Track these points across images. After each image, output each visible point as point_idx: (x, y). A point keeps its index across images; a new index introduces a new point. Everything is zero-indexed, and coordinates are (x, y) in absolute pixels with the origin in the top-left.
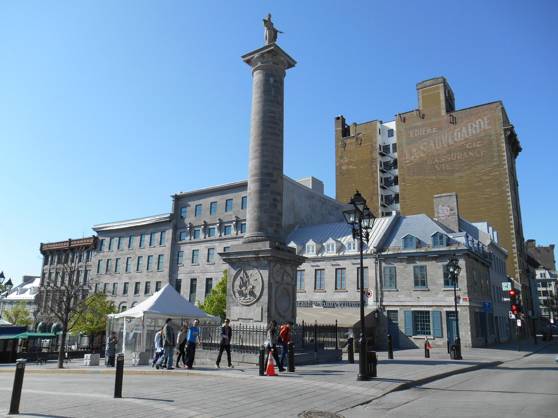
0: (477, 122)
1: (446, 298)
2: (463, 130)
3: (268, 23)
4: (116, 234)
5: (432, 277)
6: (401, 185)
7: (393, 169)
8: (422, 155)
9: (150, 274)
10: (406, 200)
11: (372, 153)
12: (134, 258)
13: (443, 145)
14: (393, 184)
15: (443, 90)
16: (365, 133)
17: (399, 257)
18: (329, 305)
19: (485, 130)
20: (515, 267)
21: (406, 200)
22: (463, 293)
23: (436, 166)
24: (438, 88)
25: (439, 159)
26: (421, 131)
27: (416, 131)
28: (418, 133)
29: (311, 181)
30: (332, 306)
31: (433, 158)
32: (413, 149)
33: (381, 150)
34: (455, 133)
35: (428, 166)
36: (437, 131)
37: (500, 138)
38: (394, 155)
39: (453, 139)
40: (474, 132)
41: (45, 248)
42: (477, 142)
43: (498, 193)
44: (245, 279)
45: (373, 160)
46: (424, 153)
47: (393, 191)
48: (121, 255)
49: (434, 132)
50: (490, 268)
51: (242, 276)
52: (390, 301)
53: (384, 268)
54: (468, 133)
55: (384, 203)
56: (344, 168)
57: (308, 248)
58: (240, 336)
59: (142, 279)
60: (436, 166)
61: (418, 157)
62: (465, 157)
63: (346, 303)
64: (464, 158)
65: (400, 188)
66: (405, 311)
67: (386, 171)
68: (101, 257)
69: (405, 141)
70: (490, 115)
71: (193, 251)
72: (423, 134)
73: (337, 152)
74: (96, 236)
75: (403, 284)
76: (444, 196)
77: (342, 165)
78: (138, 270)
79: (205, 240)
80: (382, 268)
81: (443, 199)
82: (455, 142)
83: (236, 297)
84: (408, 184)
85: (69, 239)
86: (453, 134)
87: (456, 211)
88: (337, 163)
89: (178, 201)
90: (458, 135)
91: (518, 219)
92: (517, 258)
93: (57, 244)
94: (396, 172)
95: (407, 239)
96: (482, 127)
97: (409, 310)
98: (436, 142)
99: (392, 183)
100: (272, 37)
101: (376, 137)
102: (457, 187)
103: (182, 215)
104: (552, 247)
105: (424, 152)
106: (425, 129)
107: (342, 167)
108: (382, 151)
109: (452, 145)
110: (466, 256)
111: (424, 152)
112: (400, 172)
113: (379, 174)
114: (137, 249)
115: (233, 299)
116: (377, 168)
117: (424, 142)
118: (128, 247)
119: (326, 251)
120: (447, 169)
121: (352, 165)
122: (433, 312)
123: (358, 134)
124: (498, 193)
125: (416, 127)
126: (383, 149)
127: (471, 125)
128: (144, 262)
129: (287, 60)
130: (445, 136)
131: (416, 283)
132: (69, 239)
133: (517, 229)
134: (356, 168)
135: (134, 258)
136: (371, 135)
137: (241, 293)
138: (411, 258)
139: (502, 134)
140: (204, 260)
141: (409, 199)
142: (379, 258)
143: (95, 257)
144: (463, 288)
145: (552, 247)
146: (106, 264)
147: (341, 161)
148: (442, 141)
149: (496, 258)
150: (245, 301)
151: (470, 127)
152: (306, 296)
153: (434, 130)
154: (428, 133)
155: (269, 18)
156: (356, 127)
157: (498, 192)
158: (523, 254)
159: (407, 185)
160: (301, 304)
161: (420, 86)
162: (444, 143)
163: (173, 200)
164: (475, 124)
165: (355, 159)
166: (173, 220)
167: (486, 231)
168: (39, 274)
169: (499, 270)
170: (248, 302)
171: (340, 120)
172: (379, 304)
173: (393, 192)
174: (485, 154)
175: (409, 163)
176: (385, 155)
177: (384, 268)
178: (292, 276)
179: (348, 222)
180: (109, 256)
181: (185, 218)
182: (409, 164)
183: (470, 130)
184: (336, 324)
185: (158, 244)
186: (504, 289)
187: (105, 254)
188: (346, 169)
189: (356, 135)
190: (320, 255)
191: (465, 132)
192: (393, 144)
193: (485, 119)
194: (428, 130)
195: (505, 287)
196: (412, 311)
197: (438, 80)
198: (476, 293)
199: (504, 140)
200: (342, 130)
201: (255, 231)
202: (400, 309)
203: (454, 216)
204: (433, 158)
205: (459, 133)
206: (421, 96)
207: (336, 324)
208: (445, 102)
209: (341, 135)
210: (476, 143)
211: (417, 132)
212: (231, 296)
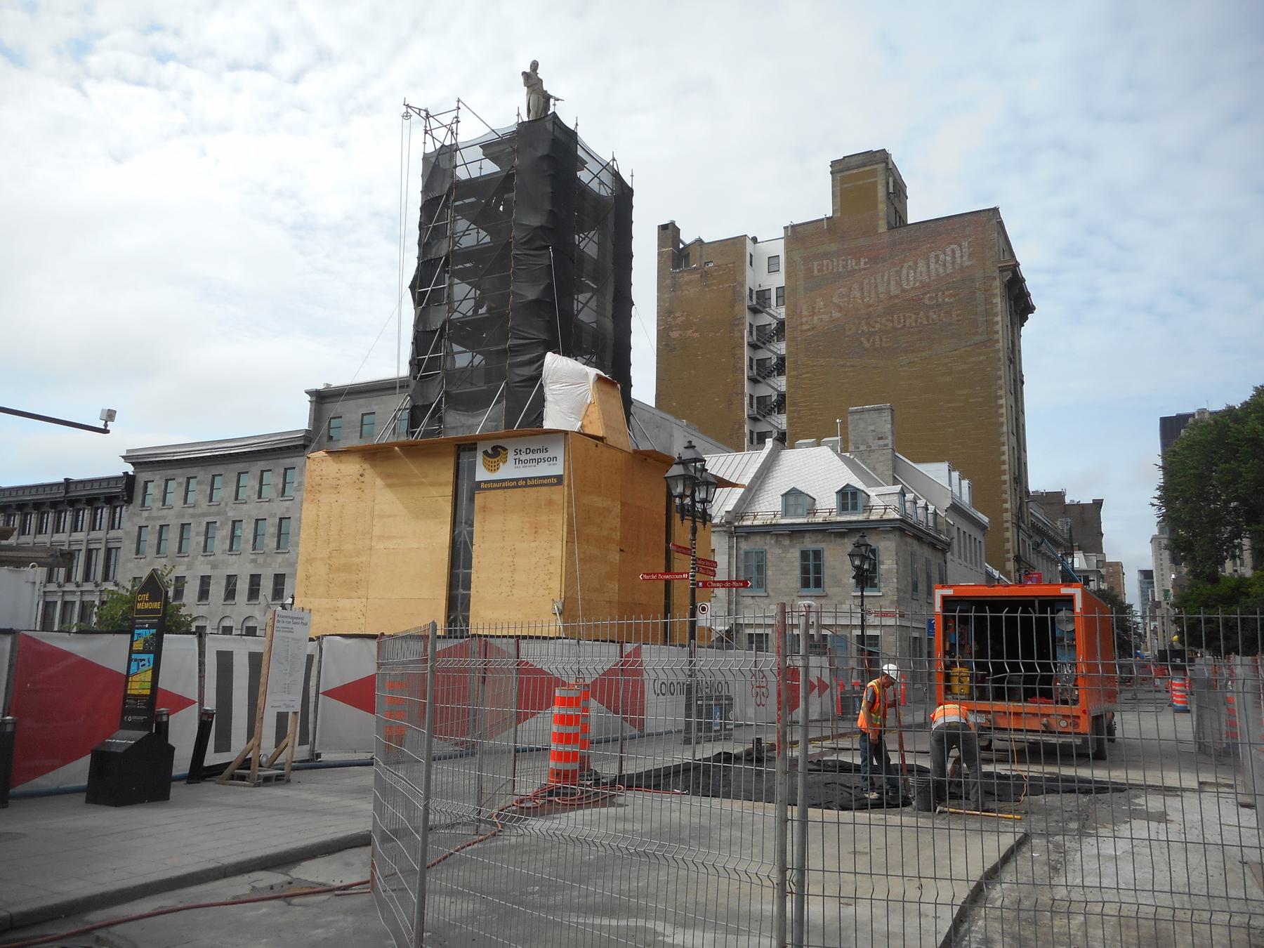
0: (948, 251)
2: (920, 265)
4: (179, 471)
5: (834, 571)
8: (836, 315)
9: (261, 559)
10: (799, 409)
11: (733, 307)
12: (222, 524)
13: (878, 294)
14: (775, 373)
15: (885, 178)
17: (774, 532)
19: (962, 268)
20: (1006, 548)
21: (799, 409)
22: (889, 602)
23: (862, 339)
24: (873, 173)
25: (869, 325)
26: (835, 263)
28: (830, 268)
31: (857, 322)
32: (817, 300)
34: (904, 272)
36: (868, 266)
37: (991, 286)
38: (778, 312)
39: (899, 283)
40: (941, 270)
42: (947, 293)
43: (980, 399)
45: (736, 322)
47: (773, 388)
48: (193, 516)
49: (862, 266)
50: (949, 554)
53: (746, 553)
54: (929, 272)
55: (756, 412)
56: (674, 335)
59: (242, 568)
60: (862, 339)
62: (922, 323)
64: (918, 324)
65: (788, 381)
67: (762, 345)
68: (144, 520)
70: (974, 237)
72: (840, 270)
74: (131, 473)
75: (779, 583)
77: (670, 328)
80: (742, 552)
81: (866, 416)
82: (904, 291)
84: (804, 373)
85: (65, 479)
86: (899, 273)
89: (322, 404)
90: (910, 276)
91: (1019, 451)
92: (1011, 530)
94: (781, 348)
95: (793, 496)
96: (958, 261)
98: (865, 289)
99: (773, 371)
100: (541, 107)
104: (1098, 504)
105: (840, 309)
106: (843, 260)
107: (671, 334)
108: (755, 302)
109: (897, 296)
110: (897, 533)
114: (230, 504)
116: (743, 338)
123: (706, 263)
124: (980, 399)
125: (827, 255)
126: (758, 298)
127: (937, 256)
128: (246, 531)
130: (883, 276)
131: (805, 583)
132: (65, 479)
133: (1014, 473)
134: (699, 336)
136: (734, 267)
138: (795, 532)
139: (995, 279)
141: (805, 406)
142: (735, 533)
143: (130, 518)
144: (890, 593)
145: (1098, 504)
146: (157, 535)
147: (669, 319)
148: (876, 287)
149: (962, 534)
151: (933, 260)
153: (862, 263)
154: (849, 268)
157: (982, 397)
158: (1023, 522)
159: (804, 376)
164: (945, 254)
167: (945, 483)
169: (968, 555)
173: (773, 390)
174: (960, 318)
175: (809, 330)
176: (762, 312)
177: (746, 553)
180: (164, 518)
181: (339, 440)
183: (932, 266)
185: (278, 494)
188: (678, 337)
191: (924, 270)
192: (777, 288)
193: (965, 244)
194: (849, 262)
198: (915, 602)
199: (998, 291)
203: (885, 451)
204: (857, 322)
210: (943, 294)
211: (827, 265)
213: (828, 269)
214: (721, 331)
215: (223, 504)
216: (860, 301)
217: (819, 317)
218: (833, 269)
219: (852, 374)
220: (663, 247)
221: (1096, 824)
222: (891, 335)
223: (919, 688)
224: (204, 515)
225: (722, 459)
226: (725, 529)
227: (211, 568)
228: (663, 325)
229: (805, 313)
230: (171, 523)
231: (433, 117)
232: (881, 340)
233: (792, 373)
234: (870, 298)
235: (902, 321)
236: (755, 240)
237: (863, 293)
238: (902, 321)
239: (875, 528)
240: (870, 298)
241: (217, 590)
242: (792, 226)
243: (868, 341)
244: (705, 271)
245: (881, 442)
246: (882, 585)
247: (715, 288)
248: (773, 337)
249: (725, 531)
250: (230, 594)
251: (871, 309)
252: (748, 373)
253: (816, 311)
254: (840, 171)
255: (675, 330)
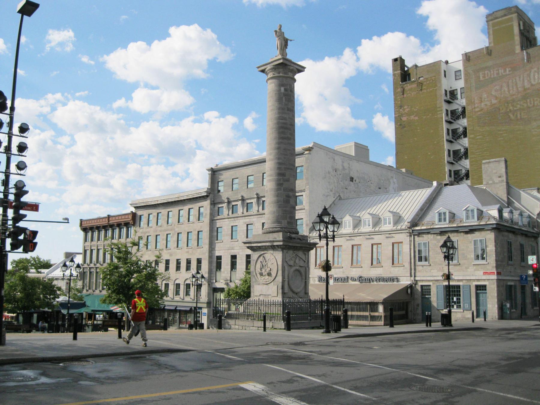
1: (476, 272)
3: (280, 34)
6: (469, 138)
7: (462, 118)
8: (494, 101)
9: (190, 250)
12: (173, 234)
15: (517, 21)
16: (427, 76)
18: (366, 280)
24: (511, 20)
25: (513, 106)
26: (492, 72)
27: (486, 72)
28: (489, 75)
29: (353, 147)
30: (368, 281)
33: (447, 97)
34: (532, 75)
35: (501, 115)
39: (529, 81)
41: (84, 225)
44: (264, 263)
46: (496, 99)
48: (161, 231)
51: (262, 261)
52: (423, 276)
53: (419, 244)
56: (404, 119)
57: (345, 223)
58: (259, 308)
61: (488, 103)
63: (336, 281)
66: (437, 286)
69: (474, 84)
71: (232, 227)
73: (395, 100)
74: (134, 212)
75: (436, 259)
76: (493, 162)
78: (178, 247)
79: (243, 215)
82: (532, 85)
83: (258, 278)
84: (478, 136)
86: (529, 75)
87: (504, 178)
88: (396, 113)
93: (96, 221)
97: (441, 284)
101: (440, 81)
102: (534, 138)
103: (219, 189)
105: (496, 98)
109: (529, 89)
111: (496, 98)
112: (469, 123)
113: (445, 126)
115: (256, 279)
117: (496, 86)
118: (166, 223)
119: (362, 226)
120: (522, 117)
121: (413, 115)
122: (463, 286)
125: (487, 68)
128: (183, 237)
129: (296, 68)
130: (520, 78)
135: (173, 234)
136: (435, 79)
137: (261, 274)
140: (243, 236)
141: (479, 154)
144: (492, 262)
147: (401, 110)
148: (516, 84)
150: (264, 281)
152: (343, 272)
154: (500, 75)
155: (280, 29)
156: (416, 69)
160: (339, 280)
161: (490, 18)
162: (518, 87)
163: (209, 174)
165: (417, 107)
166: (211, 195)
168: (81, 250)
170: (267, 282)
171: (398, 62)
172: (413, 278)
175: (479, 111)
176: (452, 103)
177: (419, 244)
178: (304, 259)
179: (316, 230)
180: (149, 232)
182: (479, 113)
184: (344, 299)
186: (530, 262)
187: (145, 230)
189: (417, 79)
190: (356, 231)
194: (500, 71)
195: (531, 260)
196: (444, 286)
197: (511, 10)
200: (401, 74)
201: (271, 224)
202: (433, 284)
203: (503, 184)
204: (506, 105)
205: (536, 74)
206: (491, 30)
207: (344, 299)
208: (520, 36)
209: (400, 80)
211: (488, 73)
212: (254, 276)
213: (488, 76)
214: (430, 115)
215: (173, 225)
216: (507, 93)
217: (485, 103)
218: (491, 75)
219: (505, 135)
220: (395, 71)
221: (30, 263)
222: (526, 111)
223: (514, 312)
224: (165, 230)
225: (411, 193)
226: (407, 231)
227: (170, 256)
228: (397, 114)
229: (476, 101)
230: (152, 235)
231: (132, 247)
232: (521, 114)
233: (472, 136)
234: (513, 91)
235: (532, 102)
236: (447, 62)
237: (509, 89)
238: (532, 102)
239: (483, 229)
240: (513, 91)
241: (173, 265)
242: (466, 54)
243: (513, 115)
244: (419, 82)
245: (500, 179)
246: (488, 258)
247: (425, 91)
248: (460, 116)
249: (407, 232)
250: (178, 268)
251: (514, 97)
252: (446, 138)
253: (483, 100)
254: (492, 20)
255: (404, 116)
